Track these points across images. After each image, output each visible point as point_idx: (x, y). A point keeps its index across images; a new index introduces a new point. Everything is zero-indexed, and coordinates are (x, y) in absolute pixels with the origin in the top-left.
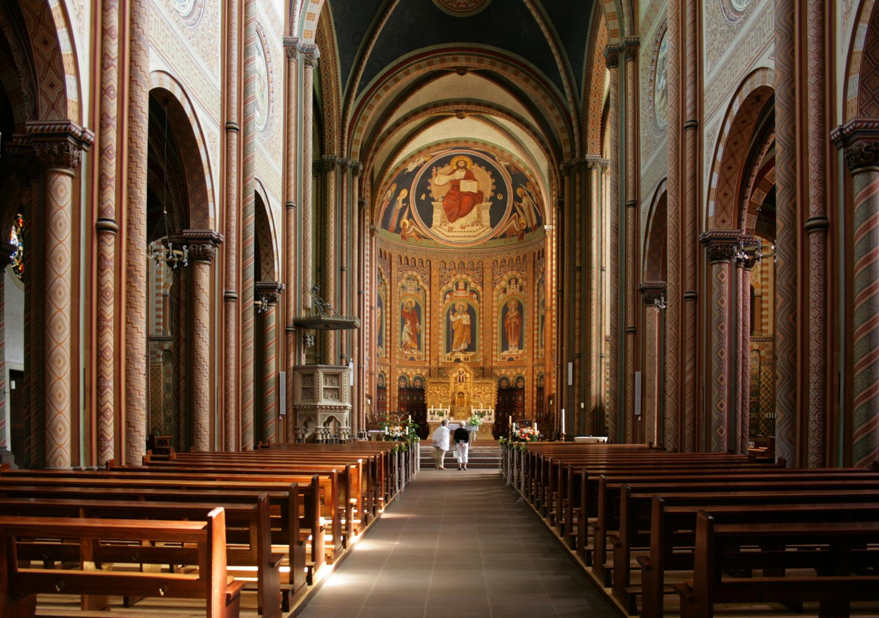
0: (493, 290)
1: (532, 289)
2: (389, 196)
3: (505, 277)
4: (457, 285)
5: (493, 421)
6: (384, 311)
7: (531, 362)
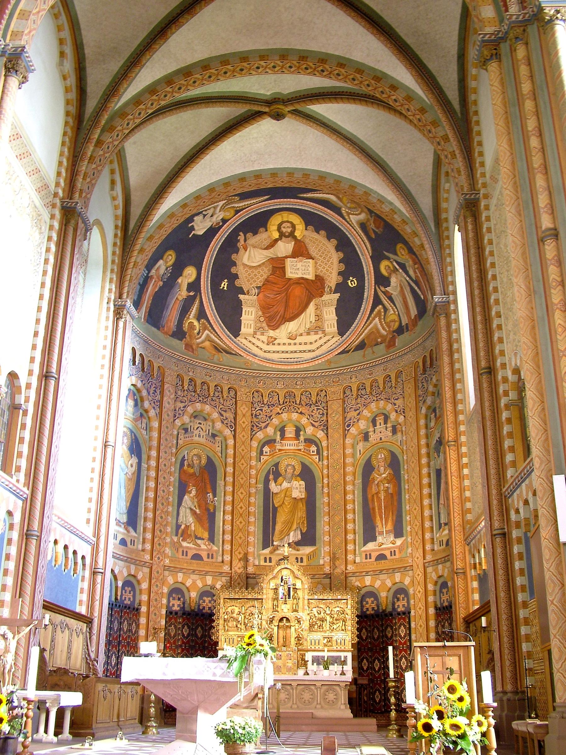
0: (345, 436)
1: (414, 426)
3: (366, 413)
4: (282, 431)
5: (349, 676)
6: (144, 465)
7: (421, 558)
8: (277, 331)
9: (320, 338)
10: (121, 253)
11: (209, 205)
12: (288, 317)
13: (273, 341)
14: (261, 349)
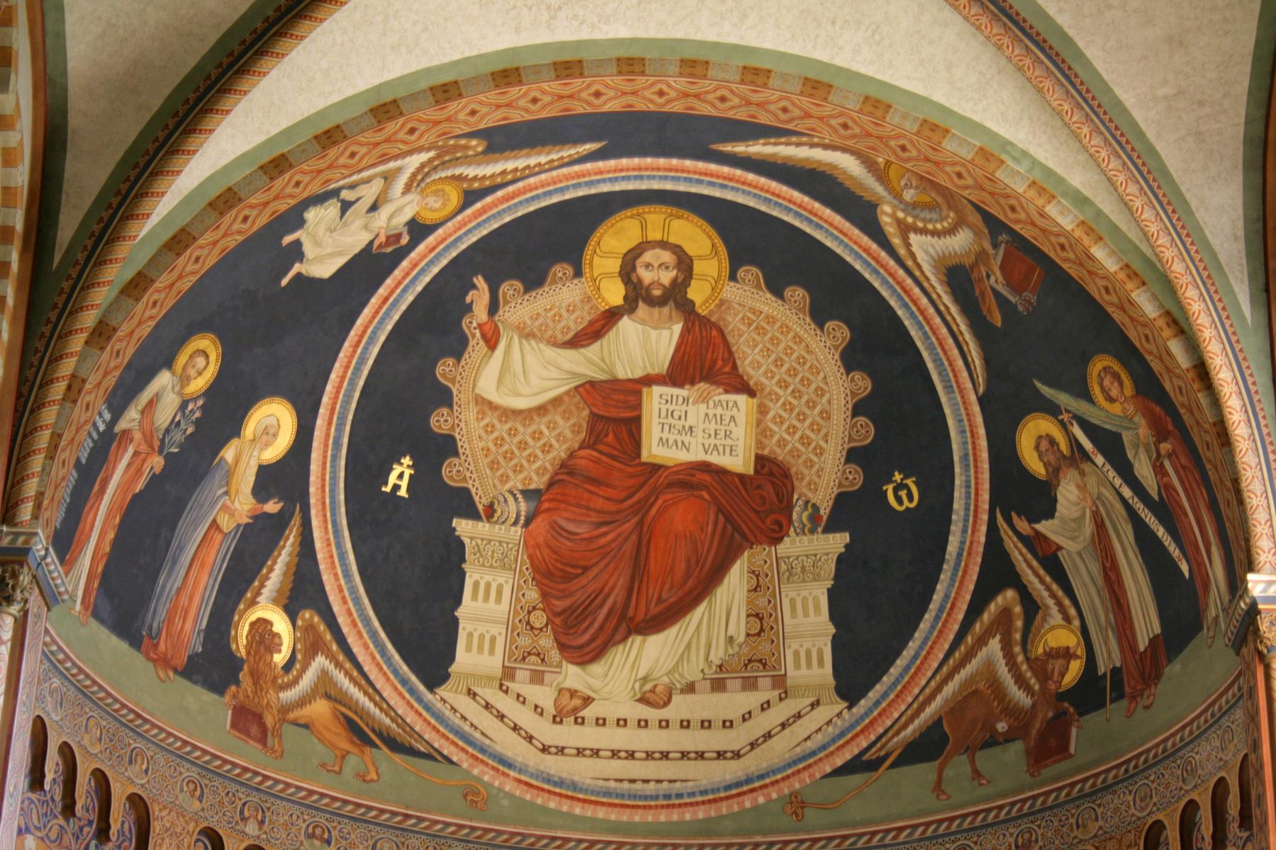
2: (165, 414)
8: (597, 668)
9: (765, 706)
10: (19, 340)
11: (373, 165)
12: (640, 616)
13: (576, 710)
14: (530, 739)
